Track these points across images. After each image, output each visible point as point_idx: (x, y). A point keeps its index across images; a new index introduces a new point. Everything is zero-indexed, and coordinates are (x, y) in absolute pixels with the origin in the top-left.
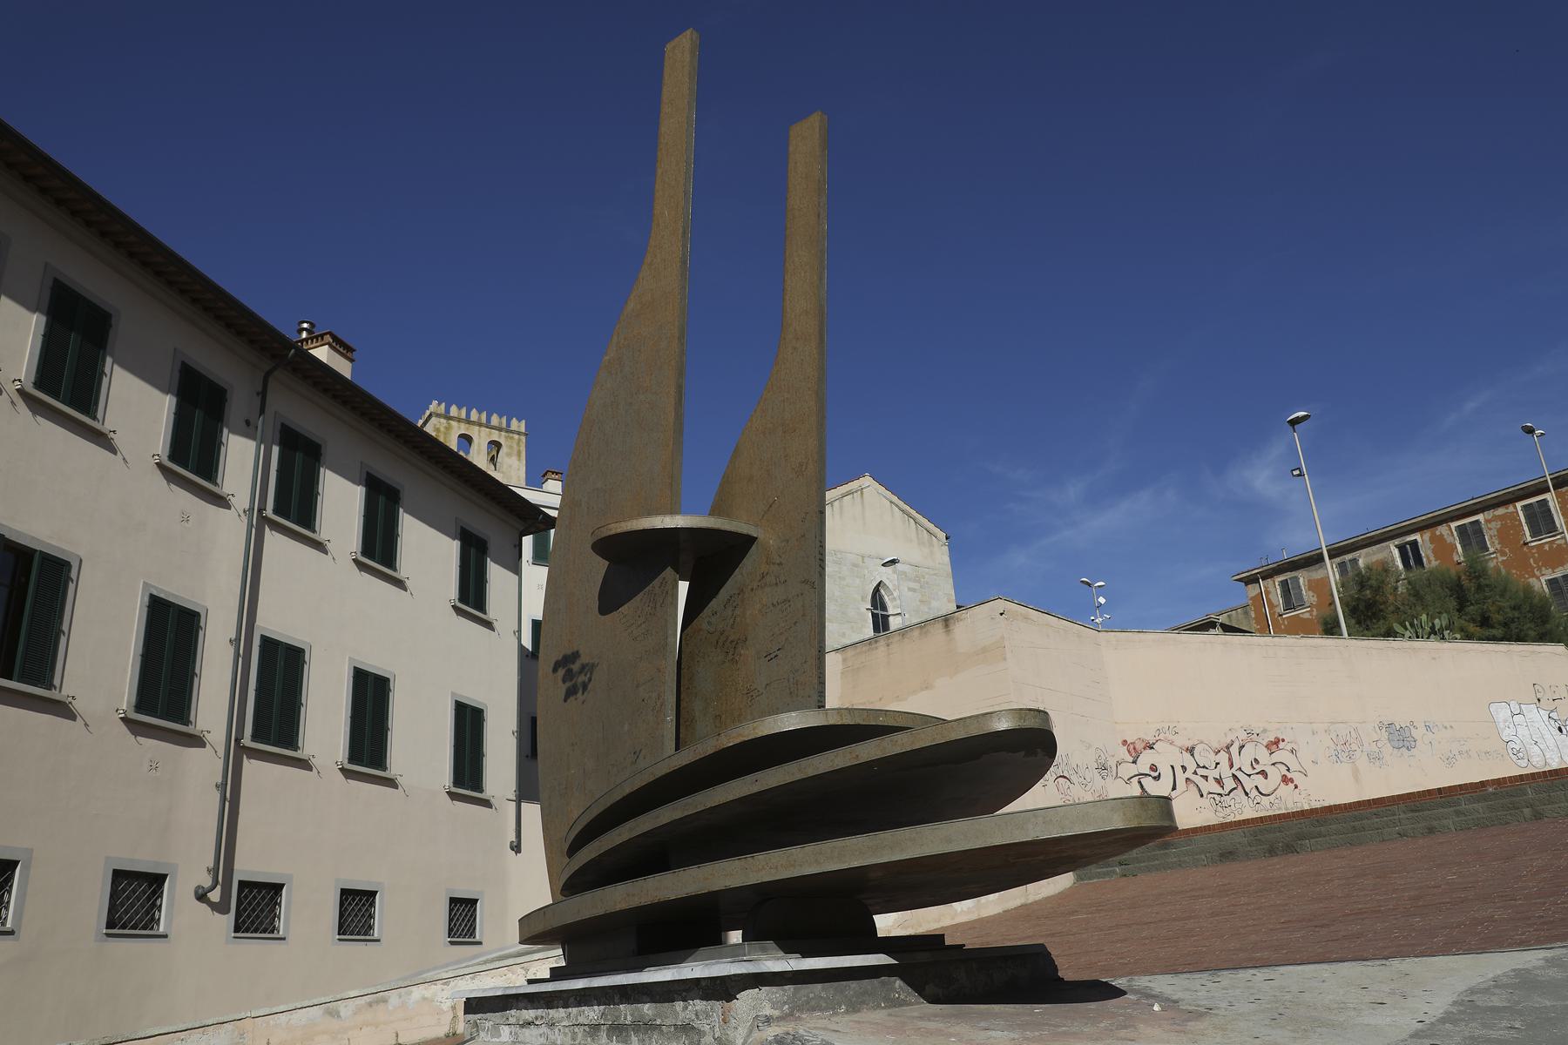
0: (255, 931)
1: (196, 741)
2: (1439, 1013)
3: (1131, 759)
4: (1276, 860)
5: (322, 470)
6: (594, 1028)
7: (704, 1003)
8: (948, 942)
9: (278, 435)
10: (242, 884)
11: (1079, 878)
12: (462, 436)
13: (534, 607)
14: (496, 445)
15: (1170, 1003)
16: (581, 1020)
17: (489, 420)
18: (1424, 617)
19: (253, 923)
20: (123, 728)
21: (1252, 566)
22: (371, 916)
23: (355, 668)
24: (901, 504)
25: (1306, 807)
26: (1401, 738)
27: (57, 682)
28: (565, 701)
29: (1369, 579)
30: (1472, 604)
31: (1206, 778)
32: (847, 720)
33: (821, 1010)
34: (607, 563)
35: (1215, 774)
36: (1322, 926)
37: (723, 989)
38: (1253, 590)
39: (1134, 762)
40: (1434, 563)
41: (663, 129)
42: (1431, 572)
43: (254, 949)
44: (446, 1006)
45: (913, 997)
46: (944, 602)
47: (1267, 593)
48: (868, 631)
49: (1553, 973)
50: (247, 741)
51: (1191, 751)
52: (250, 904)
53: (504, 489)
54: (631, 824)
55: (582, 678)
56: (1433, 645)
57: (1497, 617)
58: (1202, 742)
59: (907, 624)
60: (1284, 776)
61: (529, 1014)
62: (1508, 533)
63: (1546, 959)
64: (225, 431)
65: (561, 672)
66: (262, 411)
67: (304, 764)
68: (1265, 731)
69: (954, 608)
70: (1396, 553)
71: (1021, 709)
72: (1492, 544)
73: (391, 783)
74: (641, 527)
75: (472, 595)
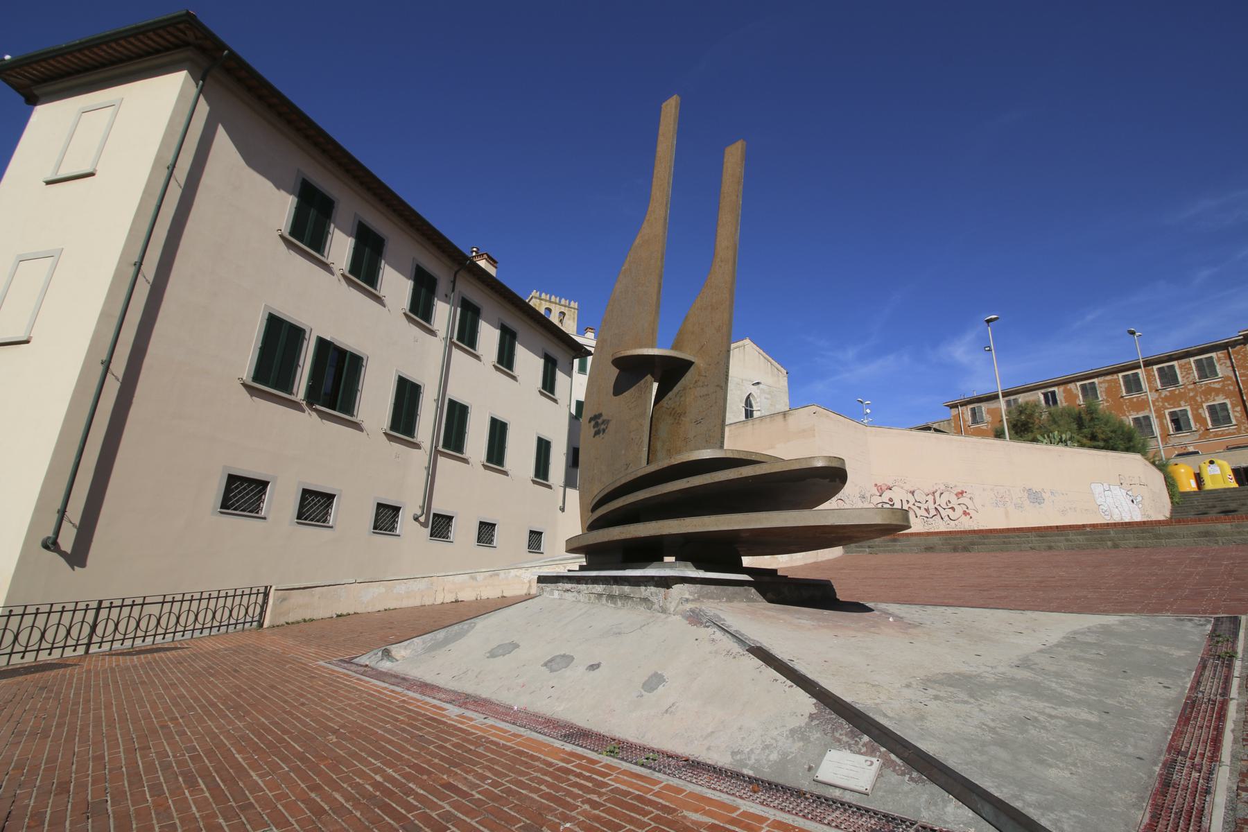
0: (440, 537)
1: (416, 446)
2: (1055, 642)
3: (879, 494)
4: (957, 554)
5: (480, 321)
6: (600, 595)
7: (656, 588)
8: (779, 574)
9: (460, 304)
10: (435, 515)
11: (846, 552)
12: (546, 308)
13: (580, 393)
14: (563, 314)
15: (899, 619)
16: (594, 591)
17: (560, 301)
18: (1056, 433)
19: (439, 533)
20: (384, 438)
21: (957, 398)
22: (493, 536)
23: (492, 417)
24: (764, 354)
25: (976, 529)
26: (1035, 497)
27: (355, 413)
28: (594, 437)
29: (1026, 409)
30: (1086, 428)
31: (920, 508)
32: (736, 456)
33: (713, 598)
34: (618, 371)
35: (924, 506)
36: (984, 591)
37: (665, 583)
38: (954, 412)
39: (880, 496)
40: (1065, 404)
41: (658, 149)
42: (1064, 409)
43: (438, 545)
44: (526, 581)
45: (760, 598)
46: (784, 404)
47: (963, 413)
48: (743, 418)
49: (1124, 628)
50: (440, 448)
51: (913, 493)
52: (438, 524)
53: (567, 335)
54: (624, 498)
55: (603, 427)
56: (1060, 448)
57: (1101, 436)
58: (919, 489)
59: (762, 415)
60: (965, 511)
61: (568, 586)
62: (1112, 391)
63: (1120, 621)
64: (436, 299)
65: (593, 423)
66: (453, 291)
67: (465, 461)
68: (956, 486)
69: (788, 409)
70: (1042, 397)
71: (830, 457)
72: (1101, 395)
73: (505, 473)
74: (636, 354)
75: (548, 385)
